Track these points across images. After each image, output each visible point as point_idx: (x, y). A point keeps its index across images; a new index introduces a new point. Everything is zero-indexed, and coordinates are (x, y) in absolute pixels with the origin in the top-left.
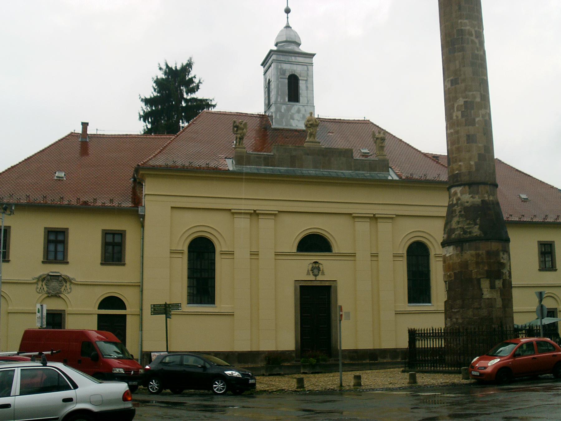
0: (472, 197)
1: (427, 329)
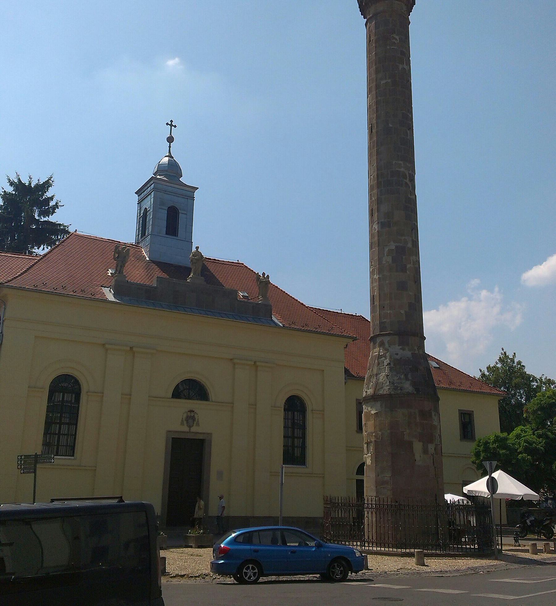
0: (401, 349)
1: (352, 498)
